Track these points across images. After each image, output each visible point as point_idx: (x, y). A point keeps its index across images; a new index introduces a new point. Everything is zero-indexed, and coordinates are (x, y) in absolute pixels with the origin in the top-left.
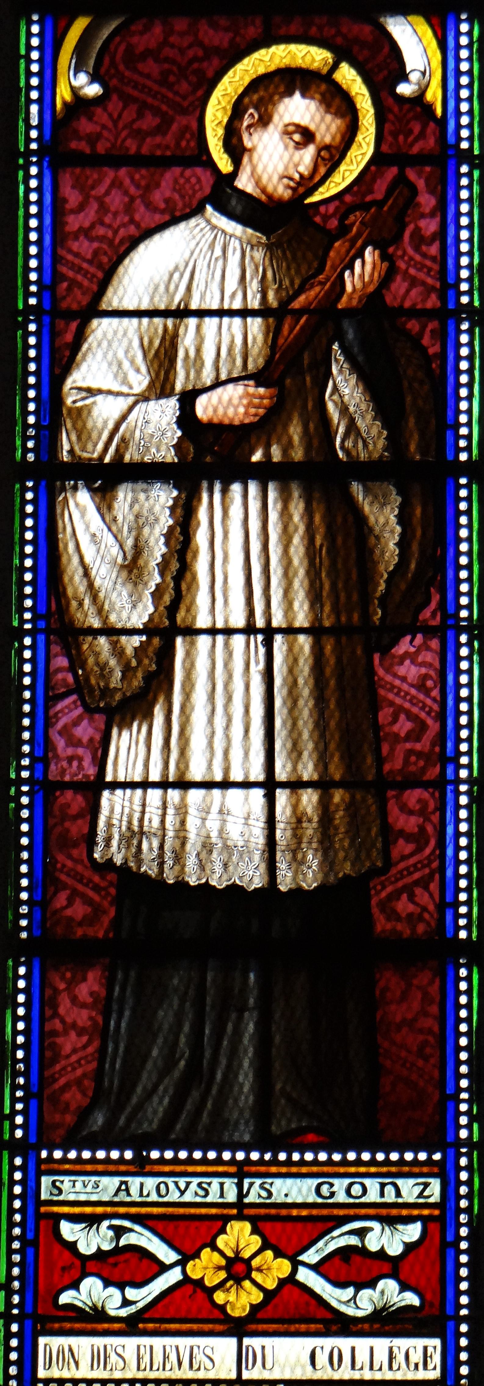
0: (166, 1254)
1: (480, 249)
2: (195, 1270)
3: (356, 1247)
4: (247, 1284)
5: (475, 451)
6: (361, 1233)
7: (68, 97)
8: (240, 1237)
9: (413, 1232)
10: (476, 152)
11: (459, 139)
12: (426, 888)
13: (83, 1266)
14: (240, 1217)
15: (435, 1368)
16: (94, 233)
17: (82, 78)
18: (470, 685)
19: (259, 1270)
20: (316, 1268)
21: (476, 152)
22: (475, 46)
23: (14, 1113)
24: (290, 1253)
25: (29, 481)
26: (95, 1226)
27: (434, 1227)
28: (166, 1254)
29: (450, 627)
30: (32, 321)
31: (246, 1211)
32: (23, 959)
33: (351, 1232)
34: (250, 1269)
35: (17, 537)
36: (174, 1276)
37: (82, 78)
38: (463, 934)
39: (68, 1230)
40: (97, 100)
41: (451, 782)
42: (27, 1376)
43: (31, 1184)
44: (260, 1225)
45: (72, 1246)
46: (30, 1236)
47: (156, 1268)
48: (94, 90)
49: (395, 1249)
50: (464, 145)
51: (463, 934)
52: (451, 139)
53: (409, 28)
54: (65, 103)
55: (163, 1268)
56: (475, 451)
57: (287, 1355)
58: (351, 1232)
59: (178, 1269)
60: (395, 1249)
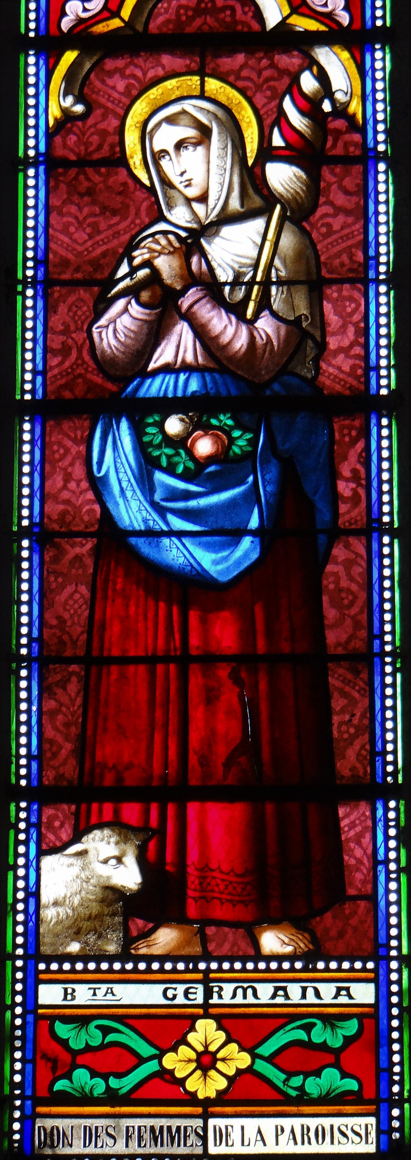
0: (145, 1049)
1: (399, 586)
2: (169, 1061)
3: (303, 1041)
4: (212, 1073)
5: (398, 643)
6: (308, 1028)
7: (58, 114)
8: (206, 1033)
9: (352, 1027)
10: (396, 525)
11: (381, 514)
12: (359, 843)
13: (74, 1059)
14: (206, 1016)
15: (372, 1143)
16: (73, 698)
17: (70, 100)
18: (392, 589)
19: (223, 1060)
20: (270, 1060)
21: (396, 525)
22: (391, 234)
23: (14, 1005)
24: (249, 1046)
25: (27, 416)
26: (85, 1028)
27: (369, 1023)
28: (145, 1049)
29: (375, 530)
30: (24, 667)
31: (212, 1011)
32: (16, 1145)
33: (298, 1027)
34: (215, 1060)
35: (14, 642)
36: (152, 1067)
37: (70, 100)
38: (379, 23)
39: (62, 1030)
40: (83, 117)
41: (379, 754)
42: (30, 1002)
43: (30, 993)
44: (225, 1022)
45: (65, 1043)
46: (33, 819)
47: (135, 1061)
48: (79, 108)
49: (336, 1043)
50: (386, 519)
51: (379, 23)
52: (371, 145)
53: (334, 58)
54: (56, 119)
55: (142, 1061)
56: (398, 643)
57: (246, 1132)
58: (298, 1027)
59: (156, 1062)
60: (336, 1043)
